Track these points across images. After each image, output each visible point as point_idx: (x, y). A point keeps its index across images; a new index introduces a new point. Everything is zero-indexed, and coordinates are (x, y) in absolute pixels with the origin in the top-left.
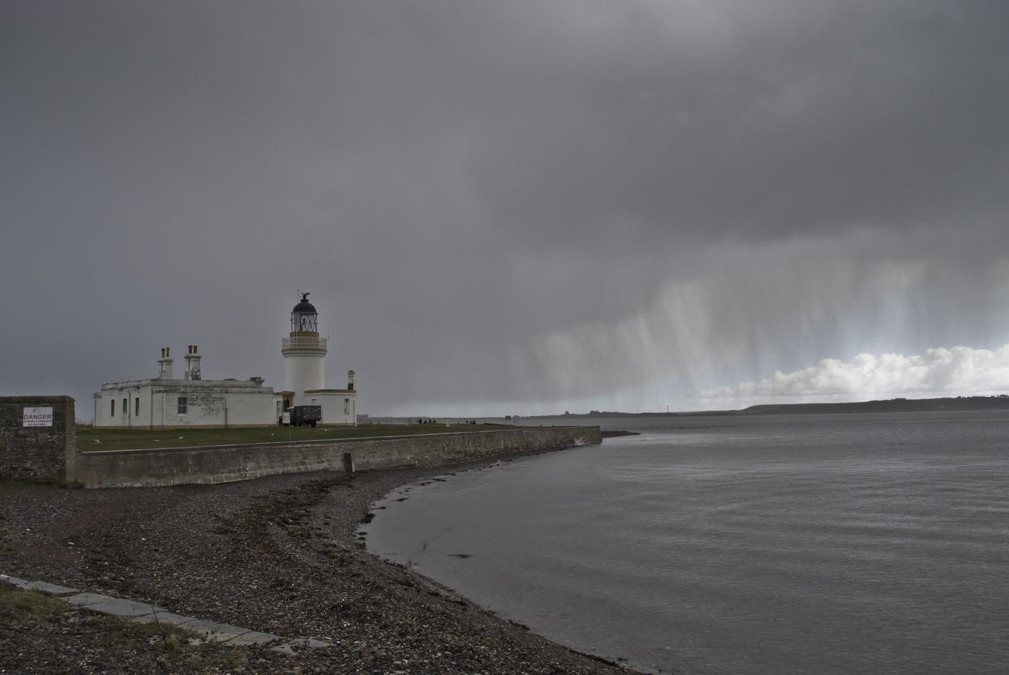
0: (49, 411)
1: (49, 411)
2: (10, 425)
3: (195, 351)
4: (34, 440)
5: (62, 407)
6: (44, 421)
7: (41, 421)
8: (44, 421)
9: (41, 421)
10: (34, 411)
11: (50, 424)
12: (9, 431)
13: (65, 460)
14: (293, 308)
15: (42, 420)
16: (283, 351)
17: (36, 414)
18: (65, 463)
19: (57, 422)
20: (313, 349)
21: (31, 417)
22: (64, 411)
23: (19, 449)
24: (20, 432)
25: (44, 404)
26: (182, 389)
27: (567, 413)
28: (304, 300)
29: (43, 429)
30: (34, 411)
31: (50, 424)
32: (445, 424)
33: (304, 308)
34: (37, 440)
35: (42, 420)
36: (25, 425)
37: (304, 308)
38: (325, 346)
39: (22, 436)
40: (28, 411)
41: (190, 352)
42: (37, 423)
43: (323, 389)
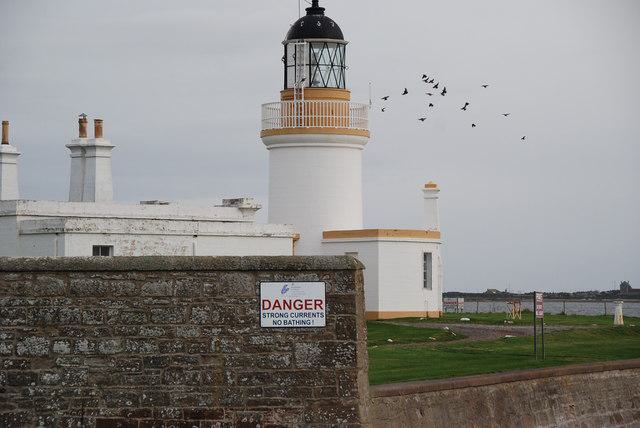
0: (316, 290)
1: (316, 290)
2: (233, 323)
3: (98, 131)
4: (286, 359)
5: (343, 278)
6: (305, 315)
7: (300, 315)
8: (305, 315)
9: (300, 315)
10: (284, 291)
11: (320, 322)
12: (231, 336)
13: (356, 406)
14: (287, 28)
15: (303, 311)
16: (265, 134)
17: (289, 297)
18: (357, 410)
19: (336, 317)
20: (319, 131)
21: (277, 304)
22: (349, 292)
23: (255, 380)
24: (255, 340)
25: (302, 275)
26: (102, 226)
27: (624, 285)
28: (315, 10)
29: (305, 333)
30: (284, 291)
31: (320, 322)
32: (612, 317)
33: (315, 28)
34: (293, 359)
35: (303, 311)
36: (266, 322)
37: (315, 28)
38: (365, 123)
39: (258, 349)
40: (270, 291)
41: (82, 131)
42: (292, 318)
43: (360, 227)
